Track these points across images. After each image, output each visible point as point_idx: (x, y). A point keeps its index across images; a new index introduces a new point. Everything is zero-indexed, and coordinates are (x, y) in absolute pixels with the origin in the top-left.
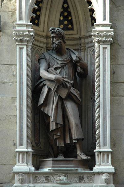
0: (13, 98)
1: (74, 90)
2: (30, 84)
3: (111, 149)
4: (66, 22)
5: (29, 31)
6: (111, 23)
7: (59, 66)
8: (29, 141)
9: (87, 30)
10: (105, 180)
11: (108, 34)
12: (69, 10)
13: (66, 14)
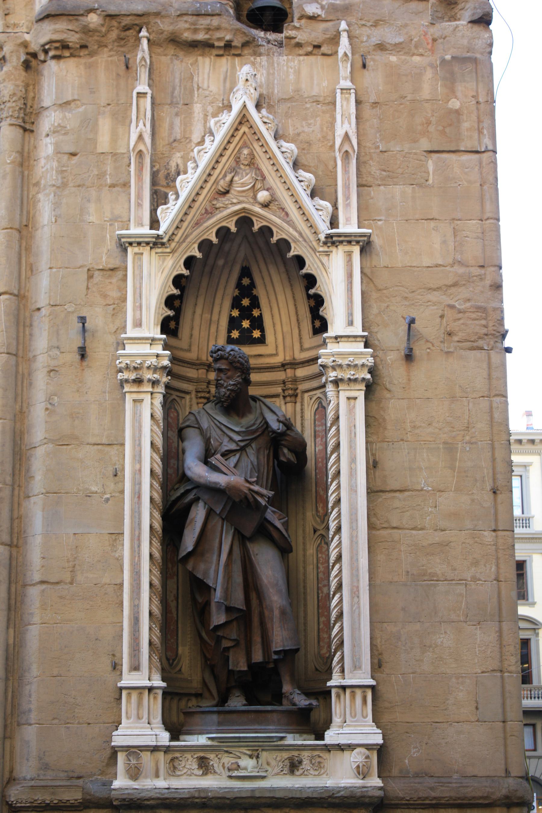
0: (114, 537)
1: (273, 512)
2: (157, 497)
3: (373, 677)
4: (246, 324)
5: (158, 356)
6: (366, 334)
7: (233, 447)
8: (156, 658)
9: (301, 346)
10: (358, 767)
11: (359, 362)
12: (254, 292)
13: (246, 302)
